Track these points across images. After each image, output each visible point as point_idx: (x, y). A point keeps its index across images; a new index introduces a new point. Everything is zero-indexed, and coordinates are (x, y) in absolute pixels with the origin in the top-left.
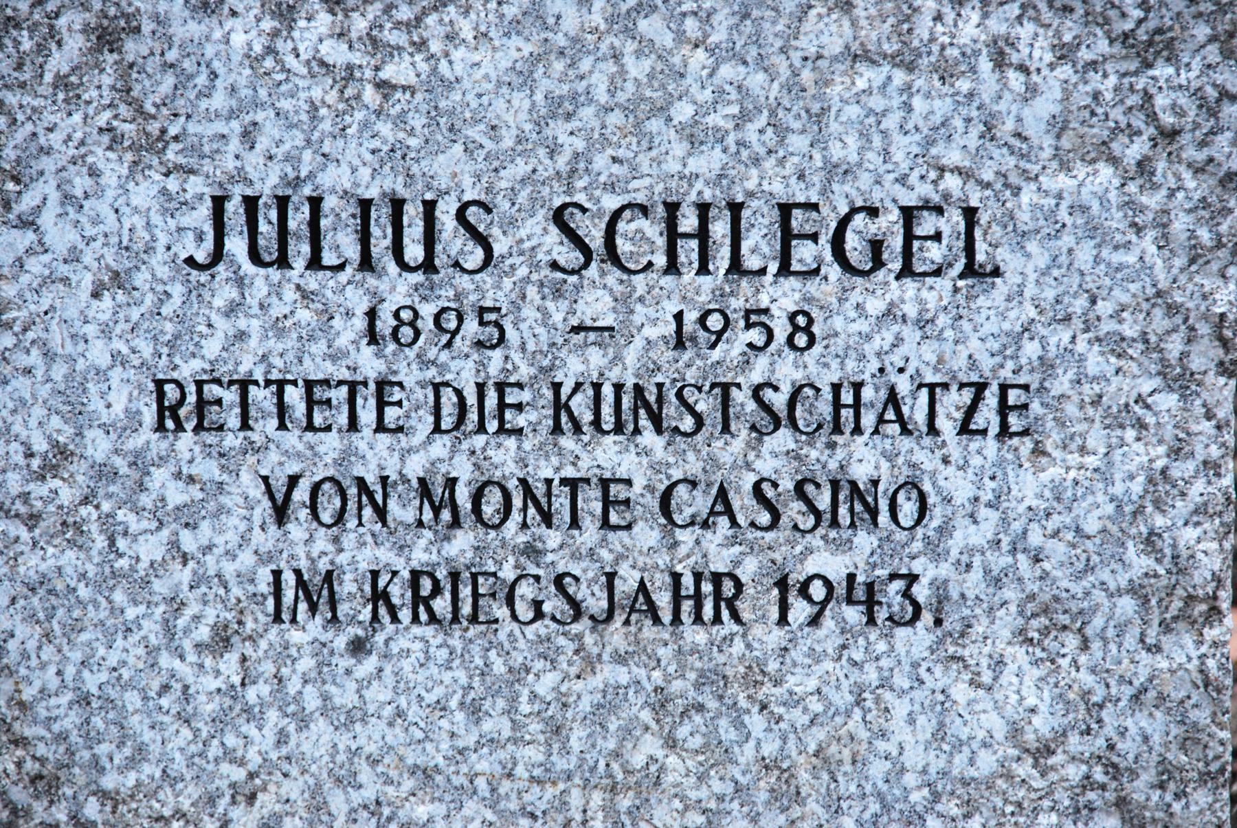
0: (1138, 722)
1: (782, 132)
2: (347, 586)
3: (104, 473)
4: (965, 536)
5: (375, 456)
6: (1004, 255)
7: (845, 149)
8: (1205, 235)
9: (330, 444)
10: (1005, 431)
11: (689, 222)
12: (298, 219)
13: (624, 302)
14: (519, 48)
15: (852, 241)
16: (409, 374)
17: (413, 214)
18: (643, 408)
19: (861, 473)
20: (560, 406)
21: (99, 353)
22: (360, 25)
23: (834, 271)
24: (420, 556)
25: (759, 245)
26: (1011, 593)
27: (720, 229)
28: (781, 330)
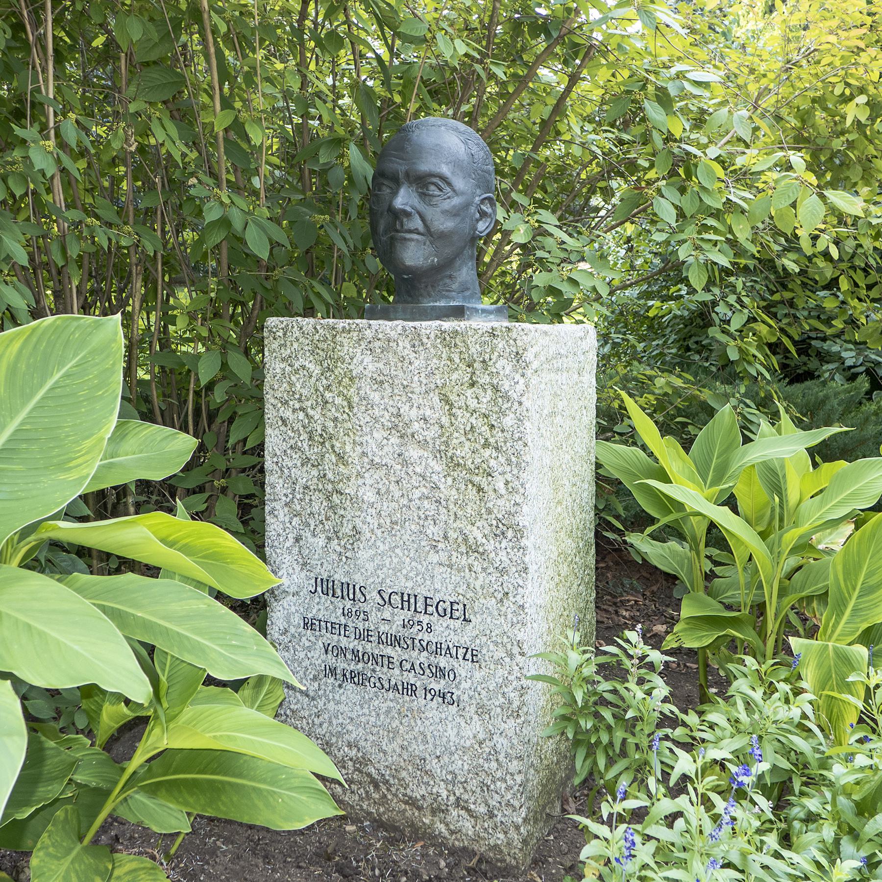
0: (501, 740)
1: (425, 580)
2: (338, 672)
3: (293, 636)
4: (464, 685)
5: (344, 642)
6: (472, 617)
7: (438, 586)
8: (515, 620)
9: (336, 637)
10: (473, 661)
11: (406, 598)
12: (330, 585)
13: (392, 614)
14: (372, 552)
15: (440, 608)
16: (350, 624)
17: (351, 587)
18: (396, 641)
19: (442, 665)
20: (379, 637)
21: (293, 609)
22: (343, 543)
23: (436, 614)
24: (352, 668)
25: (420, 606)
26: (473, 701)
27: (412, 600)
28: (425, 627)
